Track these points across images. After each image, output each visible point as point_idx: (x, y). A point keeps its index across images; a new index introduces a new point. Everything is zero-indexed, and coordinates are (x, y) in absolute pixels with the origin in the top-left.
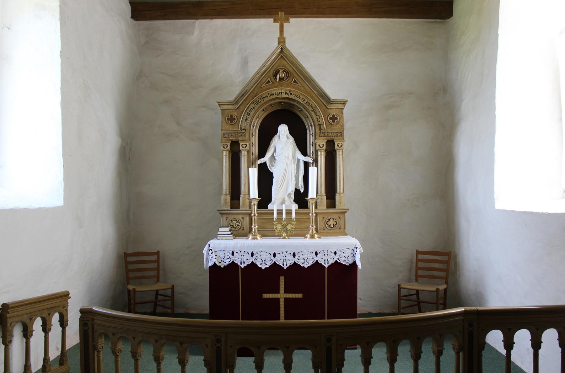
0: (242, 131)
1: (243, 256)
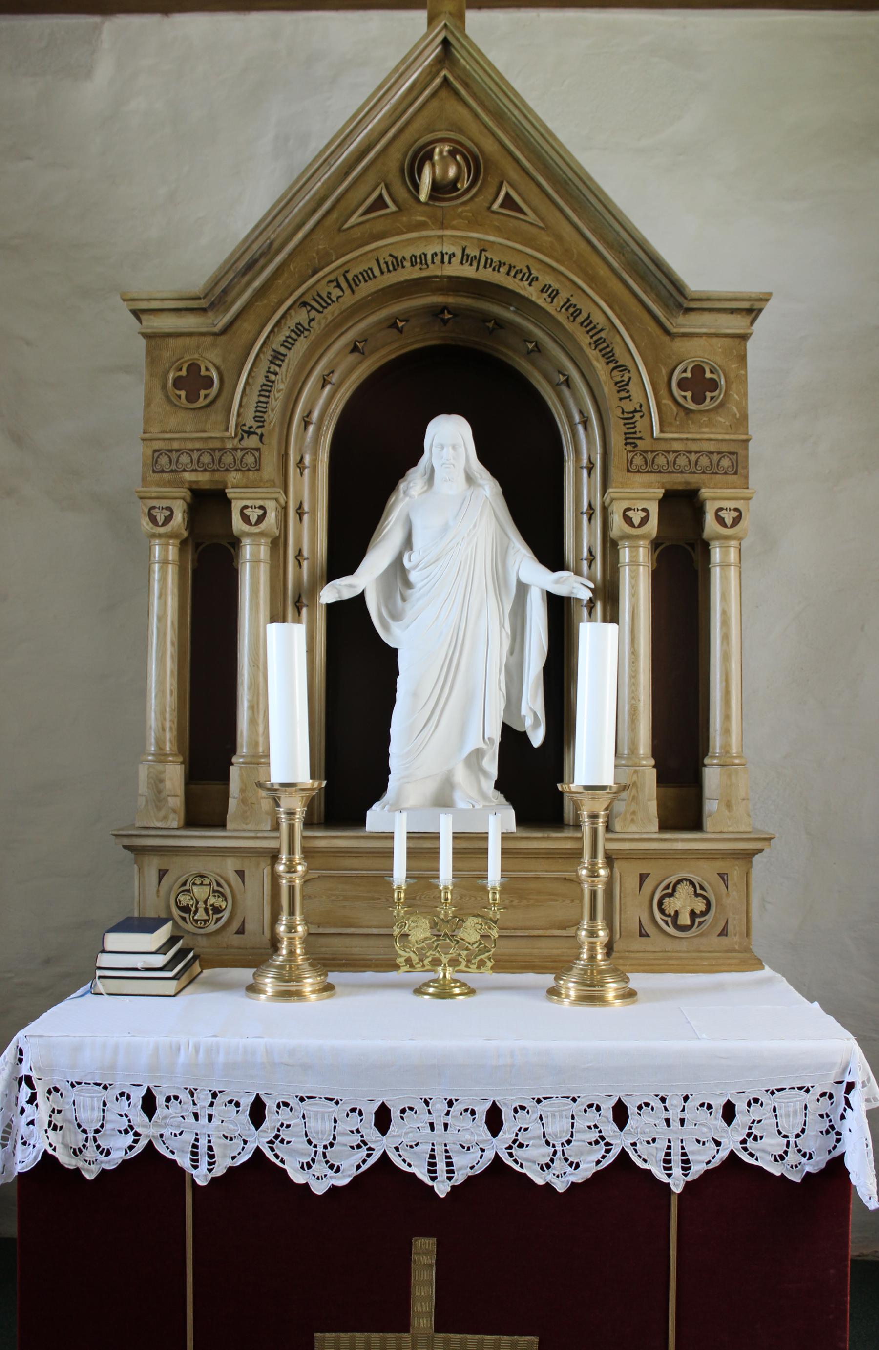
1: (204, 1120)
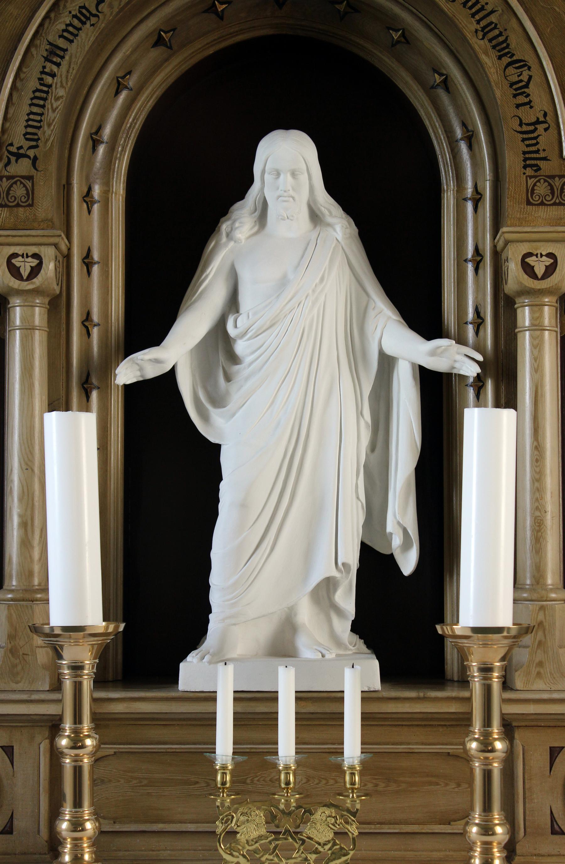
0: (13, 169)
